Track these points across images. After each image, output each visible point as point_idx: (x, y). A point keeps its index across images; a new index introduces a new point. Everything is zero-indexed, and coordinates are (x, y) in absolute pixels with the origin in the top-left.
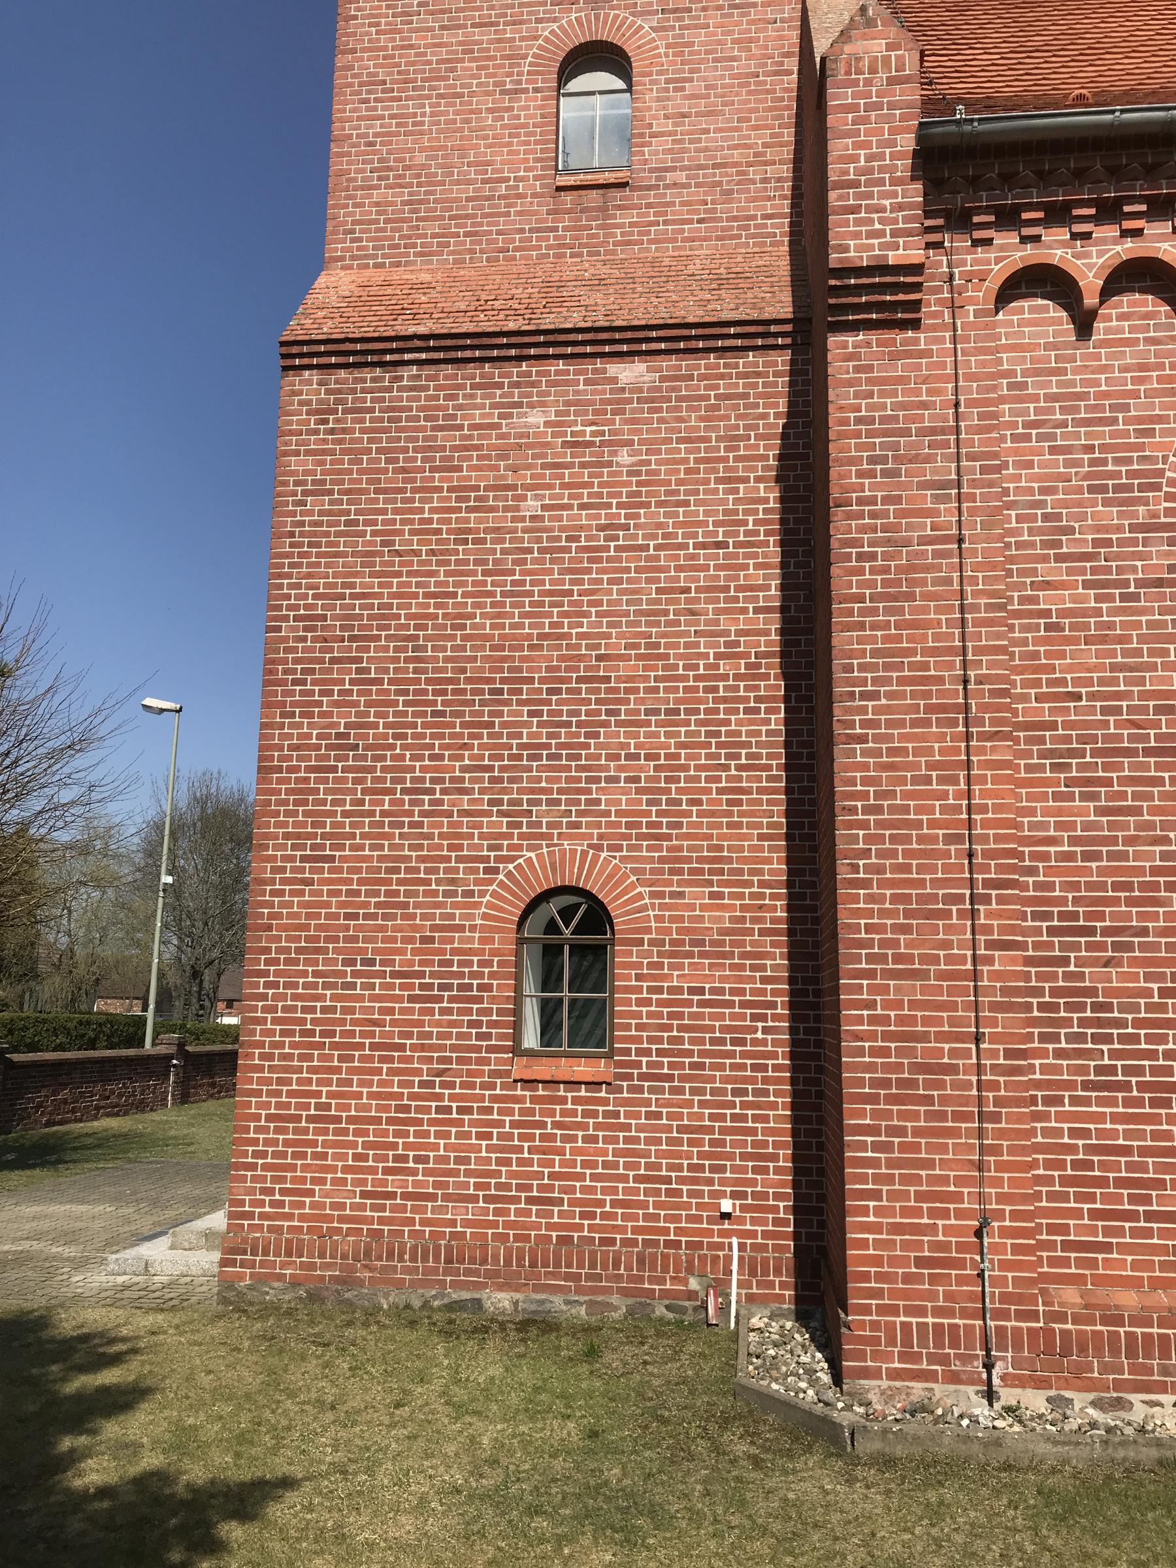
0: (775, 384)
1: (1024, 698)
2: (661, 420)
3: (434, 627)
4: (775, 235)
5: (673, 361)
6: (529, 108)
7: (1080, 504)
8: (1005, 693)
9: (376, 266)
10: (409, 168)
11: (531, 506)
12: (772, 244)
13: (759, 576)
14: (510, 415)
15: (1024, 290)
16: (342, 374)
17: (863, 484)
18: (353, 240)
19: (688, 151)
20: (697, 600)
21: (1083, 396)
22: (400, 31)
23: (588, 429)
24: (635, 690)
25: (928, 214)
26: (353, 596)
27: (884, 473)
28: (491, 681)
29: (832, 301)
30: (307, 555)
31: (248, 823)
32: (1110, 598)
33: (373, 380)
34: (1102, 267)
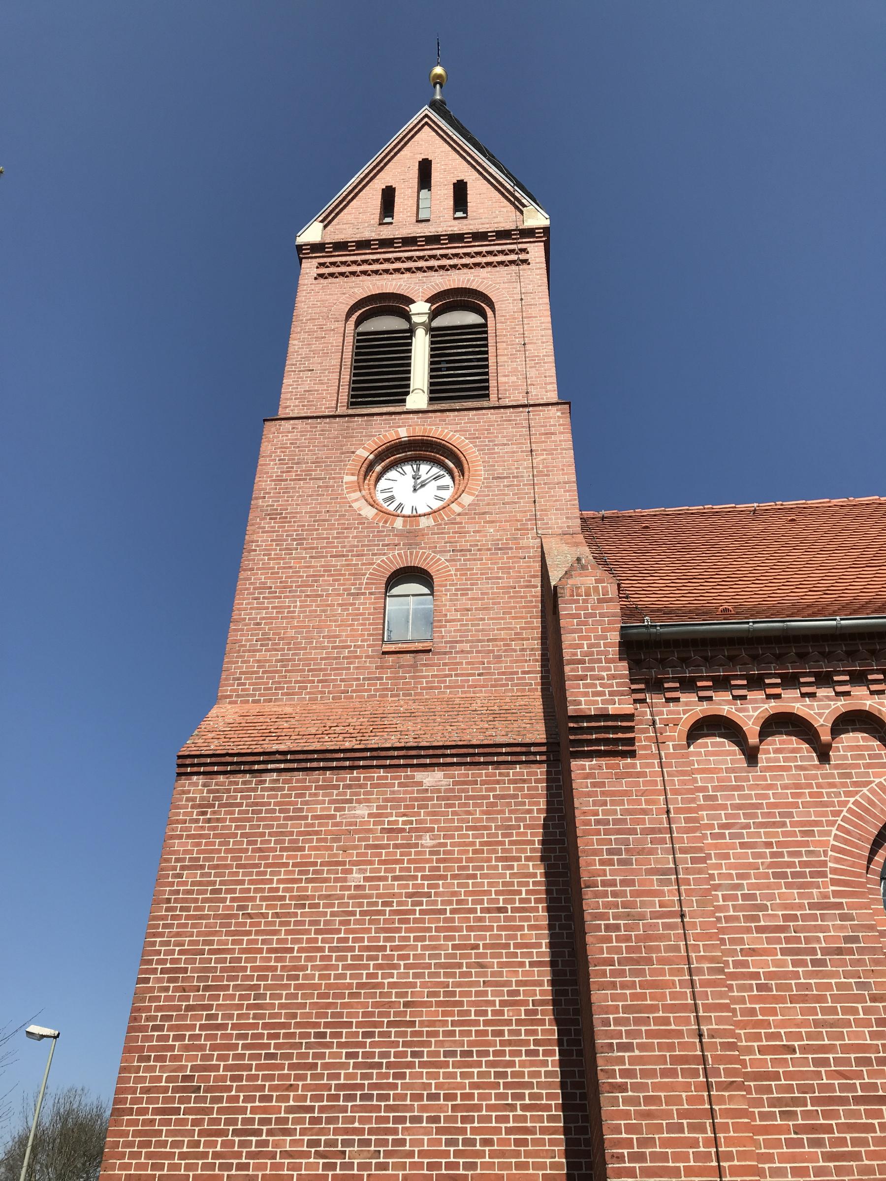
0: (537, 788)
1: (749, 1050)
2: (454, 813)
3: (274, 978)
4: (531, 684)
5: (463, 770)
6: (366, 604)
7: (768, 886)
8: (732, 1046)
9: (254, 702)
10: (283, 639)
11: (356, 877)
12: (529, 690)
13: (532, 936)
14: (343, 809)
15: (705, 731)
16: (221, 778)
17: (605, 870)
18: (239, 685)
19: (471, 631)
20: (484, 955)
21: (758, 806)
22: (284, 559)
23: (401, 819)
24: (435, 1034)
25: (633, 681)
26: (211, 952)
27: (620, 862)
28: (316, 1025)
29: (572, 737)
30: (178, 917)
31: (103, 1135)
32: (803, 963)
33: (244, 783)
34: (757, 718)
